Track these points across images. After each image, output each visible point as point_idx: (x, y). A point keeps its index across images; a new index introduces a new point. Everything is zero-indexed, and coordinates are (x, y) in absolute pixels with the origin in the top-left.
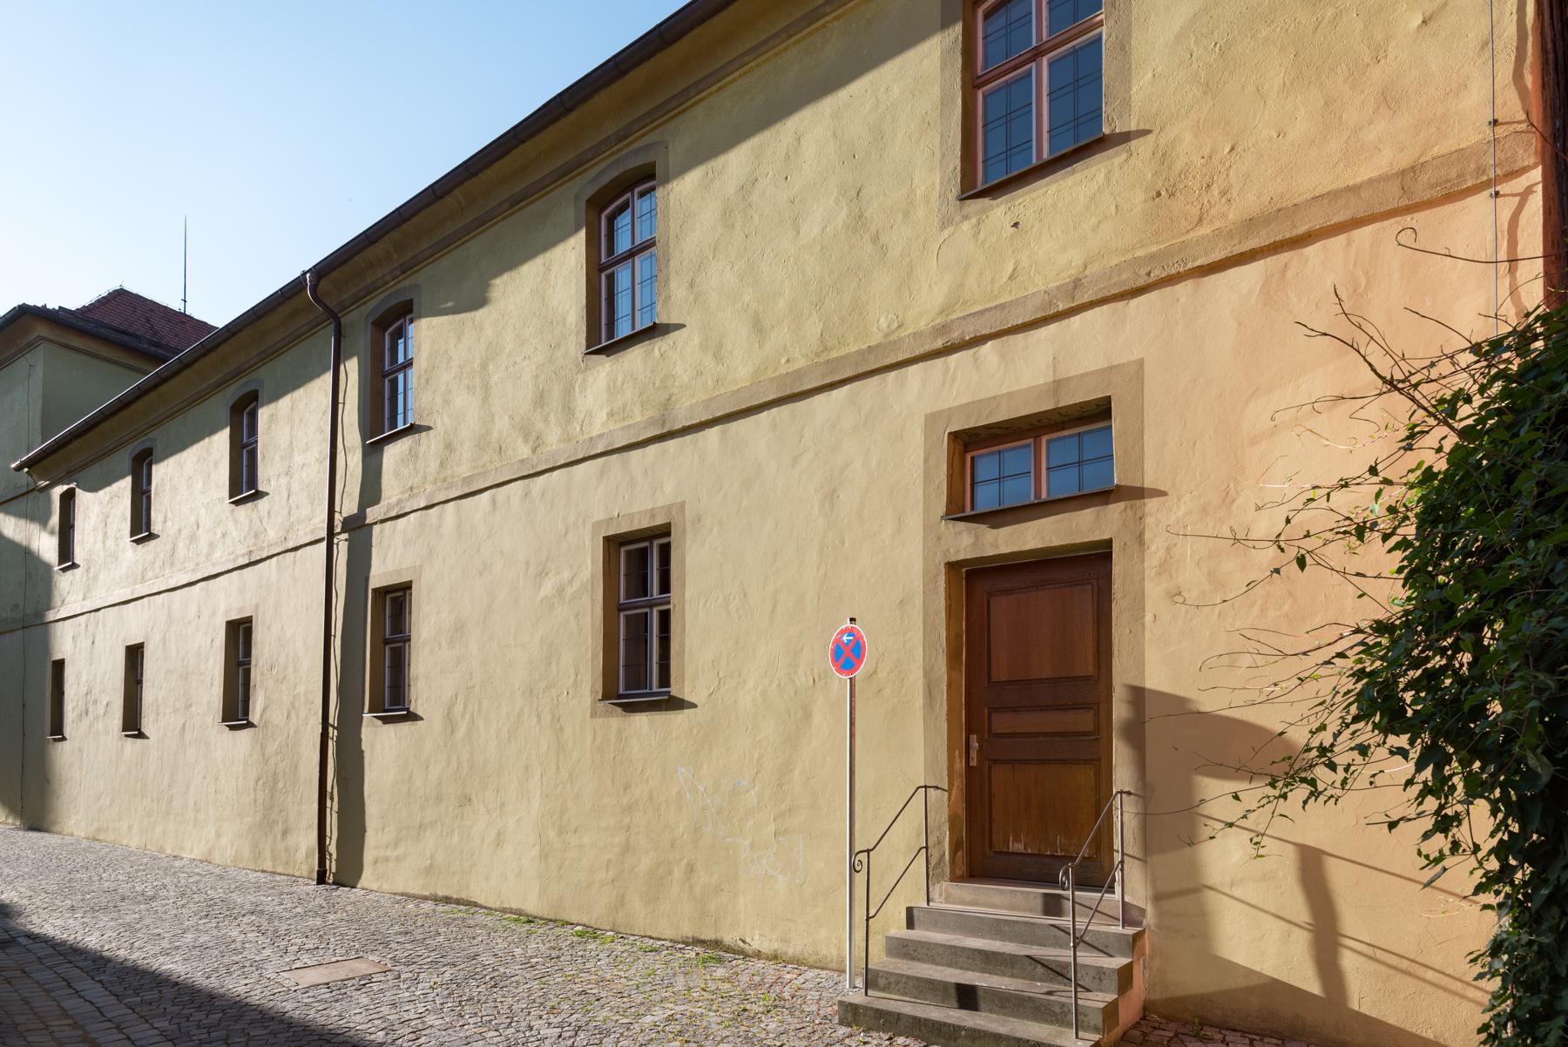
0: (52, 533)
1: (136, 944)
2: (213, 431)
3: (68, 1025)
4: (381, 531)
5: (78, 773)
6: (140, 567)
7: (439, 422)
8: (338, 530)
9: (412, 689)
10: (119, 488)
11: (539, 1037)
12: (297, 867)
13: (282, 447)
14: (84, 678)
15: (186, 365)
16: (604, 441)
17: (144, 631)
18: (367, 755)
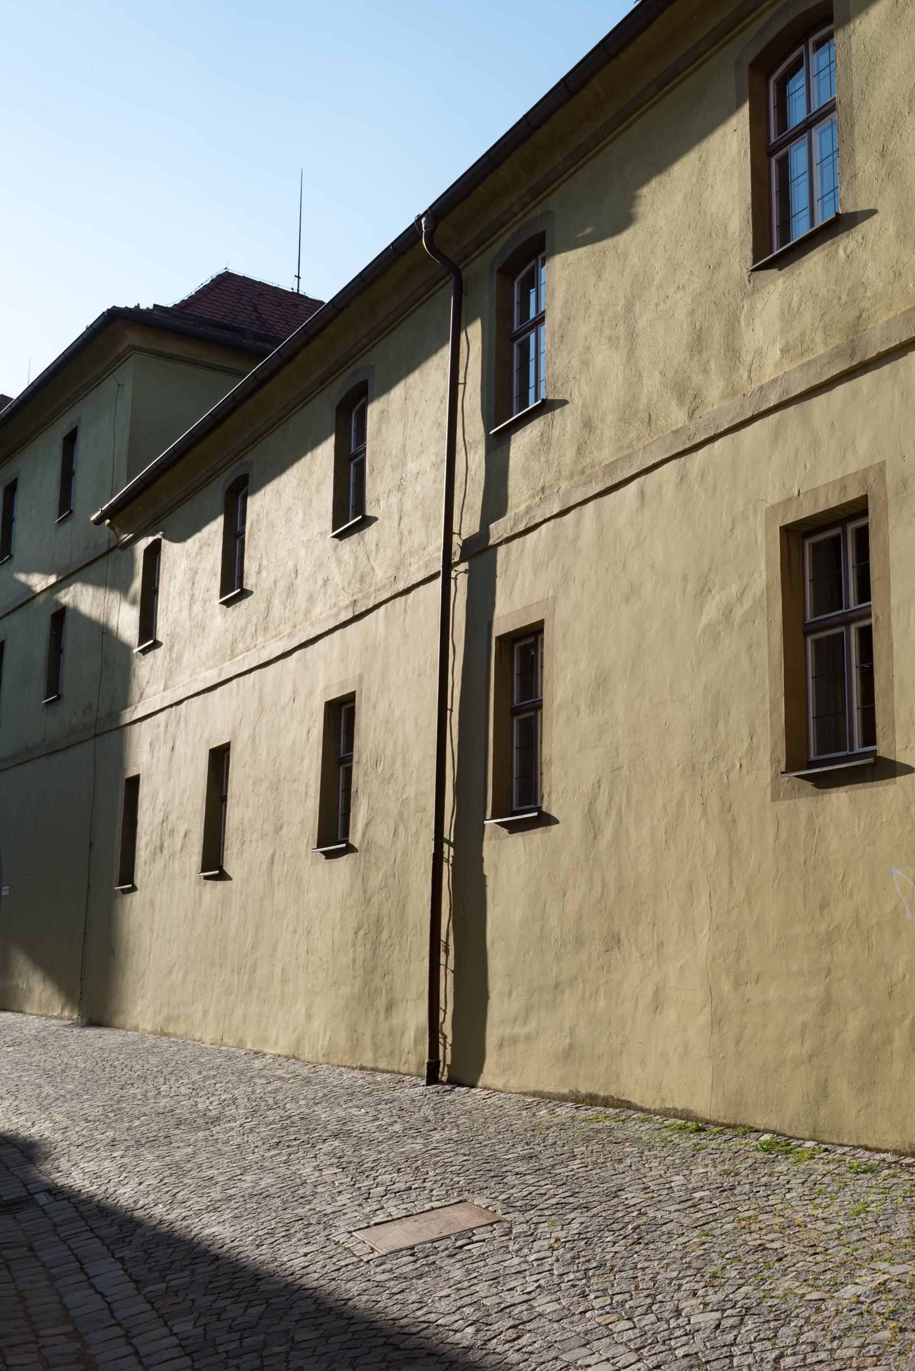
0: (133, 603)
1: (179, 1197)
2: (315, 443)
3: (64, 1334)
4: (508, 553)
5: (148, 936)
6: (230, 638)
7: (576, 393)
8: (456, 559)
9: (545, 778)
10: (210, 532)
11: (688, 1328)
12: (403, 1060)
13: (393, 453)
14: (160, 800)
15: (287, 359)
16: (778, 388)
17: (230, 726)
18: (490, 882)
